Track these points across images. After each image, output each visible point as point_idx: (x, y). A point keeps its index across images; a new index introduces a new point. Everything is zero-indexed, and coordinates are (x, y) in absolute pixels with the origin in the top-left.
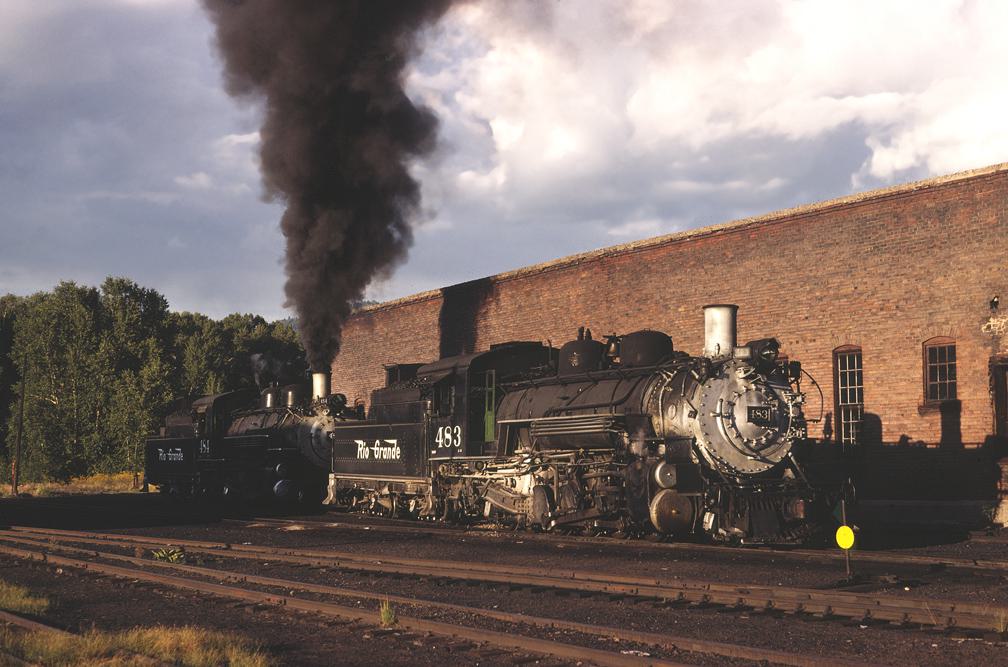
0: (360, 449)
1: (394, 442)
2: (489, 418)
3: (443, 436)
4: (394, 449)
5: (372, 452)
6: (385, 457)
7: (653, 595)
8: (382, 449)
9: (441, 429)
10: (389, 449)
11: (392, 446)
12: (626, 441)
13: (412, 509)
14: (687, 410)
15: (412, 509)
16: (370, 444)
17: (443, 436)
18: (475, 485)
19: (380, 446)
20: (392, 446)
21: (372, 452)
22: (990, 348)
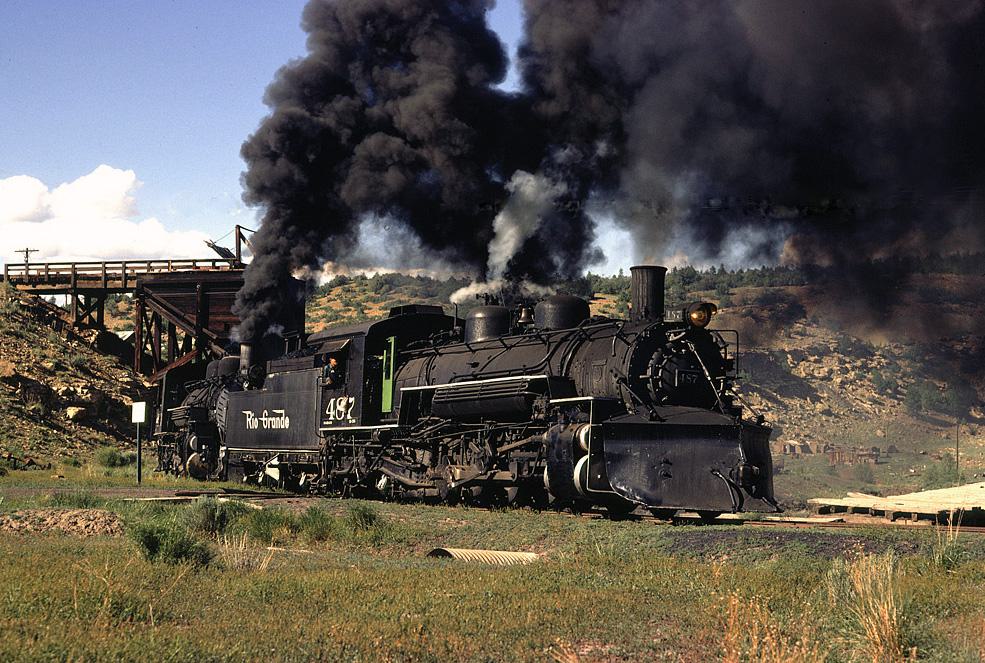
0: (249, 420)
1: (282, 411)
2: (387, 385)
3: (335, 408)
4: (282, 418)
5: (260, 422)
6: (273, 427)
7: (238, 488)
8: (270, 419)
9: (332, 400)
10: (278, 419)
11: (280, 415)
12: (562, 155)
13: (301, 483)
14: (426, 178)
15: (301, 483)
16: (258, 415)
17: (335, 408)
18: (730, 457)
19: (269, 416)
20: (280, 415)
21: (260, 422)
22: (131, 199)
